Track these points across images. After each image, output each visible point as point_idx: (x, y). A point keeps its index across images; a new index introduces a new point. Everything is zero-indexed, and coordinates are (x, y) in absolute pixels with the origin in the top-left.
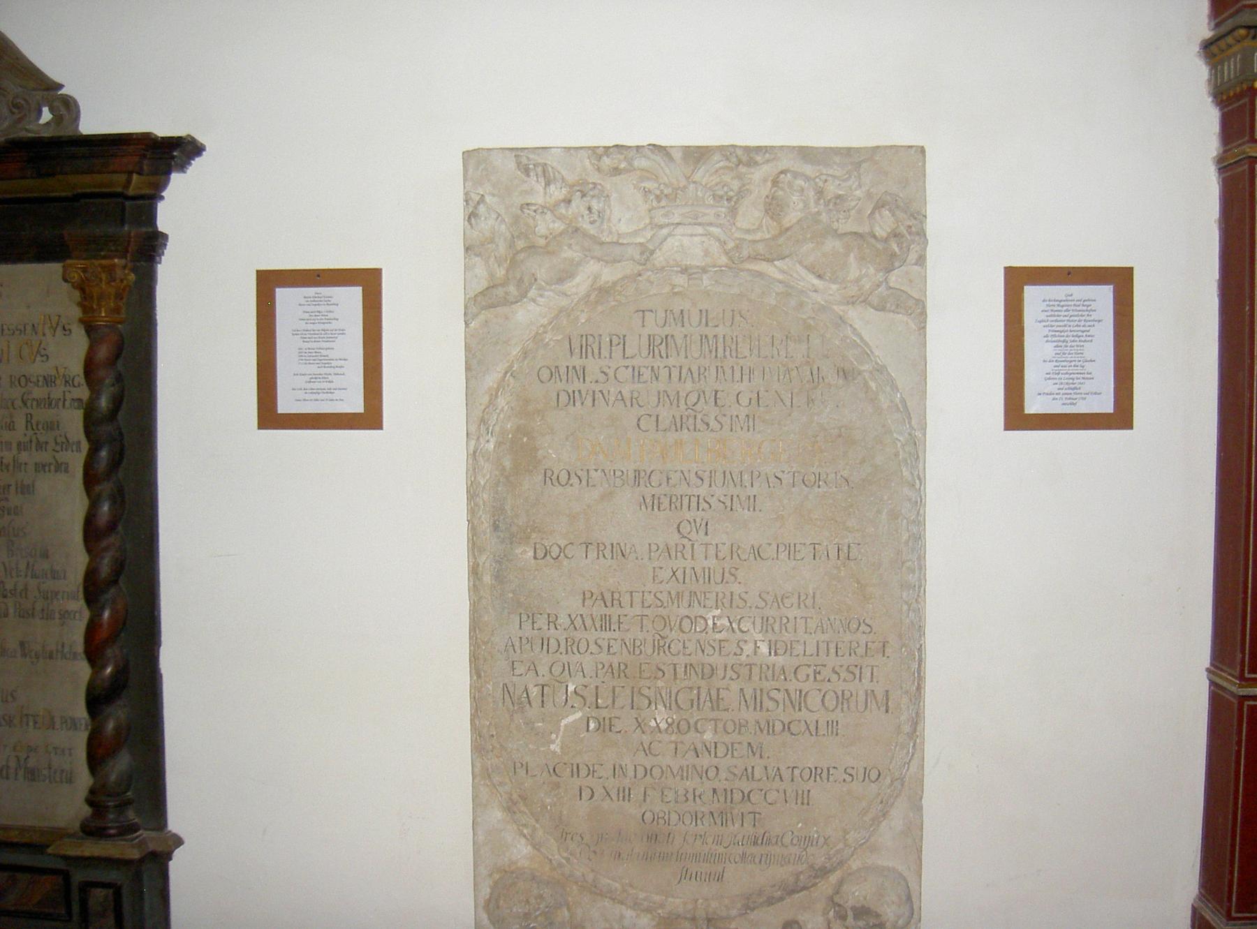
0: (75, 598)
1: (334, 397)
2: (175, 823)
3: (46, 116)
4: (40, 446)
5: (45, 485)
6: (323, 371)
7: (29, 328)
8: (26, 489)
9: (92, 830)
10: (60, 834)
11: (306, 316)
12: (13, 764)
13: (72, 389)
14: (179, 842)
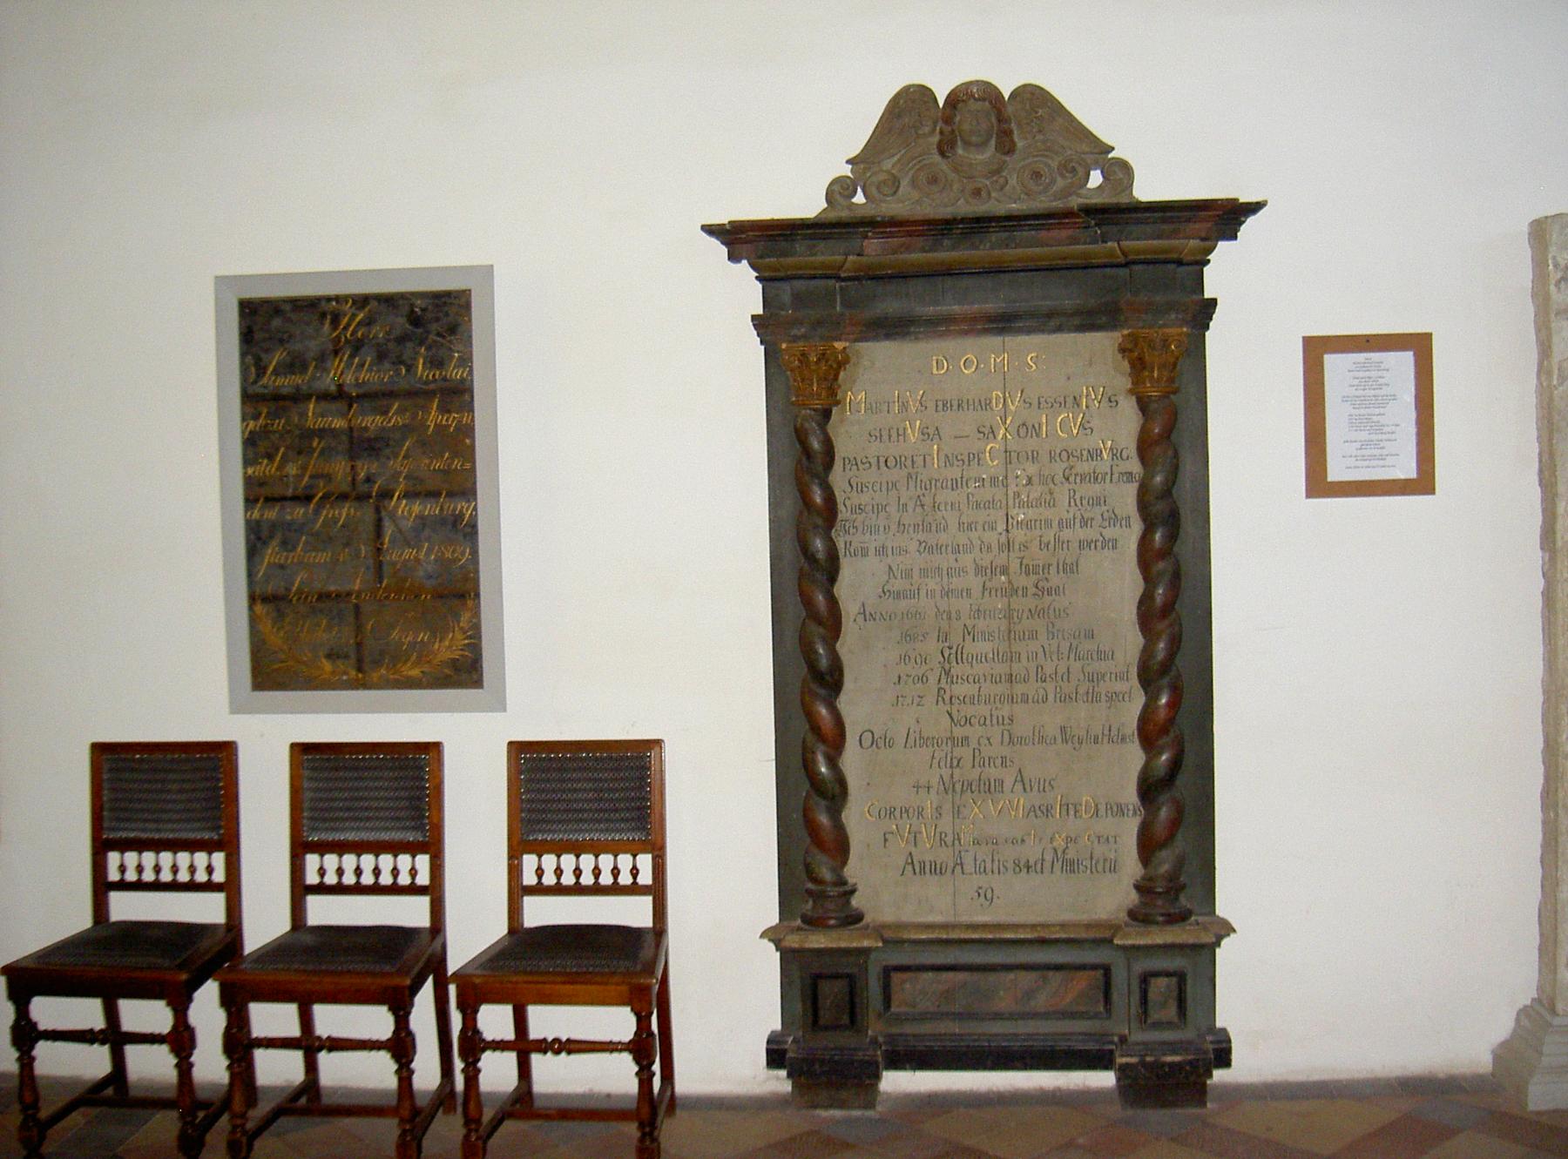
0: (1121, 677)
1: (1386, 463)
2: (1222, 909)
3: (1096, 179)
4: (1085, 523)
5: (1091, 562)
6: (1374, 437)
7: (1070, 400)
8: (1071, 568)
9: (1138, 916)
10: (1116, 928)
11: (1356, 382)
12: (1048, 857)
13: (1120, 462)
14: (1227, 929)
